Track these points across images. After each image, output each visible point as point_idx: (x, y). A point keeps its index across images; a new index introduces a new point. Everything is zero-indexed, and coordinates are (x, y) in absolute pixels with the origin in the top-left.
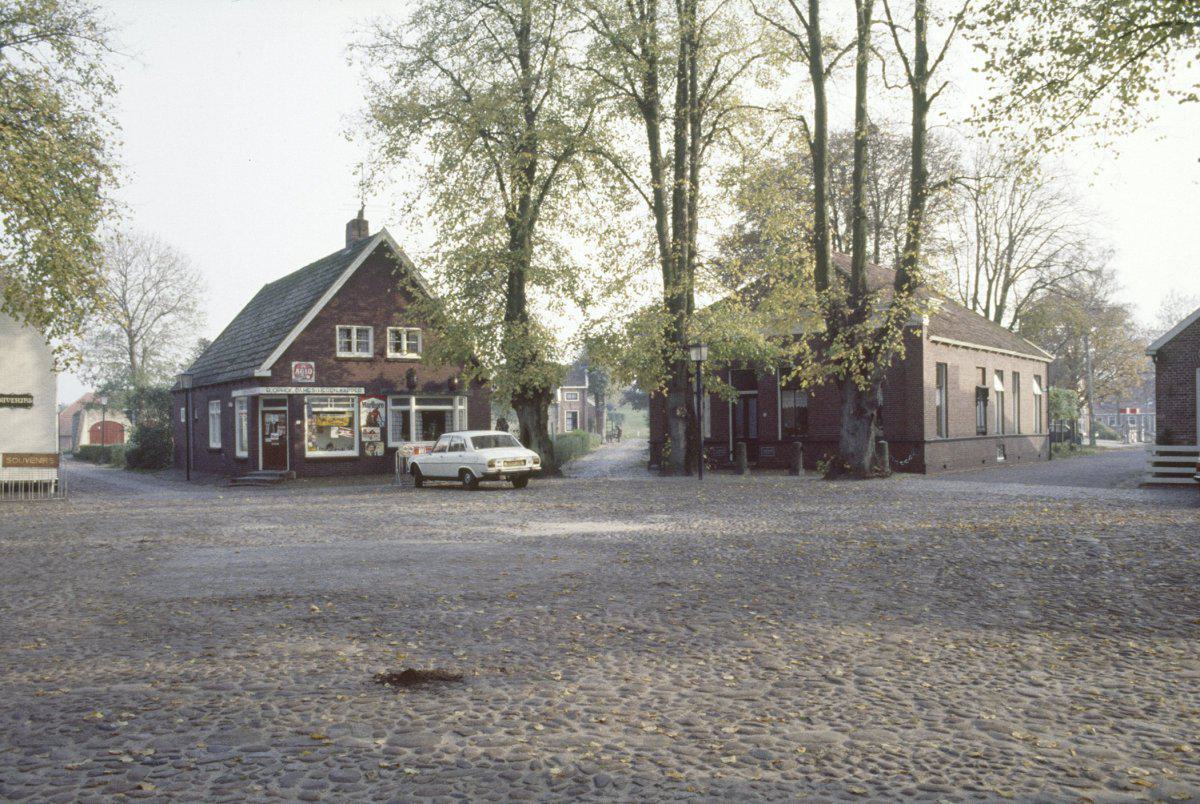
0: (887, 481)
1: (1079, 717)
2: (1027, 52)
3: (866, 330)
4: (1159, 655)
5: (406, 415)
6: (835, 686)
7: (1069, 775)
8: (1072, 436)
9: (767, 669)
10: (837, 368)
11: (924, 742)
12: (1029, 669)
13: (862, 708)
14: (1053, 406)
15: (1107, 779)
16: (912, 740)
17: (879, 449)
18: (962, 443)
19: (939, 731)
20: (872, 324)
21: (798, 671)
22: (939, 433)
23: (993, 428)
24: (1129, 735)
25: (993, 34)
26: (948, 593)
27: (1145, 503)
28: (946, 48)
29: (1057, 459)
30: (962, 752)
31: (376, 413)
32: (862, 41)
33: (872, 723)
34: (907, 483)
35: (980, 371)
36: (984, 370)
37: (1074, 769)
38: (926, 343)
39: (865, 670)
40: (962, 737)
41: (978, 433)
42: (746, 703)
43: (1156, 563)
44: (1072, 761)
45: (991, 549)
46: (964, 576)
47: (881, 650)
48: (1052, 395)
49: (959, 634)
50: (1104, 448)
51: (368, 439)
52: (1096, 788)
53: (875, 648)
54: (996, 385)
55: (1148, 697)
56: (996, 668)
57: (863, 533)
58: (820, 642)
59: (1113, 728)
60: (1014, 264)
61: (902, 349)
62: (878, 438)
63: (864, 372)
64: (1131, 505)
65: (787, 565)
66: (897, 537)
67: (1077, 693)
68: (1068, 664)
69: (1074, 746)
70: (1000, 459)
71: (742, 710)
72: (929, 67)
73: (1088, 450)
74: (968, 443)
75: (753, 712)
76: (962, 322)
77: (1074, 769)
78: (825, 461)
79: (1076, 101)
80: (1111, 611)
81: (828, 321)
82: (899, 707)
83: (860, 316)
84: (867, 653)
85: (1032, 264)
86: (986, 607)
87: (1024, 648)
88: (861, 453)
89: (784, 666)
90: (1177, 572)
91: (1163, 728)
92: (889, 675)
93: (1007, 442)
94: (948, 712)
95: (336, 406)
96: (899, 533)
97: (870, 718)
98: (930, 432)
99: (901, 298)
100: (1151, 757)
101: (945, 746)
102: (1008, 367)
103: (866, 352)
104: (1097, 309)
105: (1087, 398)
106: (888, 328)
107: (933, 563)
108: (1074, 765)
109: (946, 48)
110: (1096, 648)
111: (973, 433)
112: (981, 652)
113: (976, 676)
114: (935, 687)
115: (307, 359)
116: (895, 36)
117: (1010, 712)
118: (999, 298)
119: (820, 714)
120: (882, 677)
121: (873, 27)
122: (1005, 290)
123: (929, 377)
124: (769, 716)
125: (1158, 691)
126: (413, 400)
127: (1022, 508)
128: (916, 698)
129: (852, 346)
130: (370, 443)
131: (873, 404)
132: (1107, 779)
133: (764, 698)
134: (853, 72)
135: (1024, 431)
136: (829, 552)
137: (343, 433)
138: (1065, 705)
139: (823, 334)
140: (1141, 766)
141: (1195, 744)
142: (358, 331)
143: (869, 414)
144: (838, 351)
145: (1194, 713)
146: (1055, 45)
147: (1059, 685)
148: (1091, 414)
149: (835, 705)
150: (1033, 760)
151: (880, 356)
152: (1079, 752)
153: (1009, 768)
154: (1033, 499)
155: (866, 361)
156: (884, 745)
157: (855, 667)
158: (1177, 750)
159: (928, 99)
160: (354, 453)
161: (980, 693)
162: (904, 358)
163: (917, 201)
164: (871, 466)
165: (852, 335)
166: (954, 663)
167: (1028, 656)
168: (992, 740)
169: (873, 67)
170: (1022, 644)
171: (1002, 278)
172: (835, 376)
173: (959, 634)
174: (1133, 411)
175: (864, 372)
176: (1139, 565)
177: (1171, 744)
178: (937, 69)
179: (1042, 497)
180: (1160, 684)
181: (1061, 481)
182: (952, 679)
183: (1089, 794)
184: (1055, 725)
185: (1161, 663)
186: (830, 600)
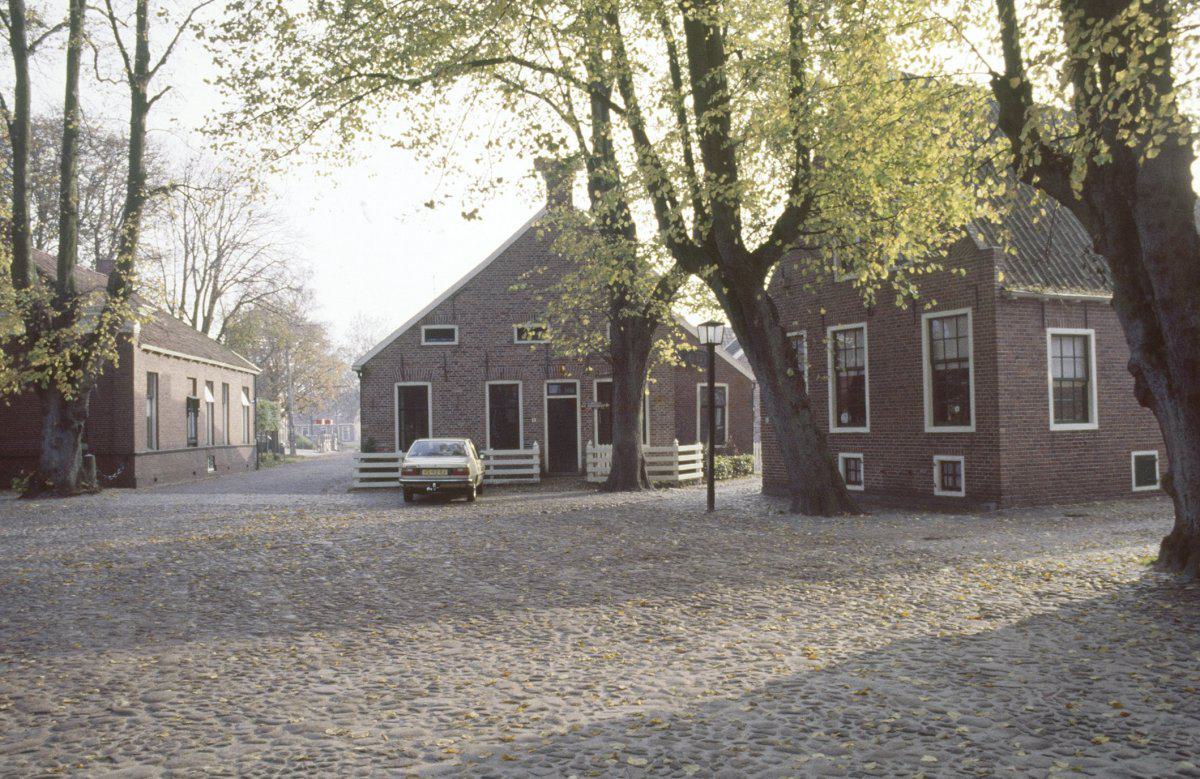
0: (95, 496)
1: (376, 705)
2: (259, 75)
3: (75, 335)
4: (422, 639)
6: (125, 719)
7: (390, 758)
8: (274, 445)
9: (36, 713)
10: (38, 376)
11: (246, 756)
12: (315, 669)
13: (166, 735)
14: (259, 416)
15: (422, 754)
16: (232, 757)
17: (86, 463)
18: (173, 455)
19: (254, 743)
20: (81, 329)
21: (76, 710)
22: (150, 445)
23: (204, 439)
24: (424, 711)
25: (234, 51)
26: (209, 607)
27: (359, 506)
28: (168, 52)
29: (263, 470)
30: (286, 759)
32: (75, 22)
33: (182, 748)
34: (116, 498)
35: (191, 382)
36: (194, 380)
37: (391, 751)
38: (137, 352)
39: (152, 696)
40: (280, 744)
41: (189, 445)
42: (24, 756)
43: (389, 560)
44: (387, 745)
45: (235, 559)
46: (218, 588)
47: (162, 673)
48: (258, 404)
49: (237, 645)
50: (303, 457)
52: (417, 764)
53: (154, 672)
54: (206, 396)
55: (427, 677)
56: (285, 674)
57: (91, 554)
58: (90, 675)
59: (410, 709)
60: (221, 279)
61: (115, 357)
62: (85, 452)
63: (72, 380)
64: (347, 509)
65: (13, 596)
66: (131, 555)
67: (366, 684)
68: (348, 659)
69: (383, 732)
70: (211, 470)
71: (23, 765)
72: (151, 67)
73: (290, 459)
74: (179, 456)
75: (39, 764)
76: (170, 331)
77: (391, 751)
78: (22, 478)
79: (300, 129)
80: (367, 607)
81: (27, 323)
82: (205, 727)
83: (67, 319)
84: (146, 678)
85: (240, 277)
86: (252, 616)
87: (304, 650)
88: (65, 467)
89: (55, 707)
90: (409, 565)
91: (450, 702)
92: (181, 696)
93: (217, 453)
94: (257, 722)
96: (131, 550)
97: (179, 744)
98: (140, 445)
99: (115, 303)
100: (450, 727)
101: (268, 756)
102: (218, 378)
103: (74, 358)
104: (296, 324)
105: (287, 409)
106: (99, 334)
107: (181, 580)
108: (391, 748)
109: (168, 52)
110: (367, 641)
111: (182, 443)
112: (264, 660)
113: (269, 683)
114: (234, 701)
116: (115, 28)
117: (315, 712)
118: (206, 310)
119: (120, 750)
120: (174, 700)
121: (88, 13)
122: (213, 302)
123: (140, 386)
124: (61, 765)
125: (432, 671)
127: (250, 516)
128: (218, 715)
129: (57, 352)
131: (80, 416)
132: (422, 754)
133: (45, 746)
134: (63, 57)
135: (234, 442)
136: (61, 578)
138: (360, 697)
139: (21, 337)
140: (445, 736)
141: (478, 709)
143: (76, 425)
144: (41, 356)
145: (467, 684)
146: (286, 73)
147: (347, 680)
148: (291, 425)
149: (134, 738)
150: (354, 751)
151: (90, 363)
152: (391, 736)
153: (336, 763)
154: (256, 508)
155: (74, 368)
156: (206, 768)
157: (140, 695)
158: (467, 718)
159: (148, 100)
161: (280, 699)
162: (117, 366)
163: (134, 205)
164: (78, 482)
165: (57, 340)
166: (243, 675)
167: (310, 657)
168: (308, 741)
169: (86, 57)
170: (301, 647)
171: (210, 289)
172: (37, 386)
173: (237, 645)
174: (328, 422)
175: (72, 380)
176: (374, 562)
177: (461, 713)
178: (158, 72)
179: (264, 506)
180: (431, 664)
181: (276, 489)
182: (247, 690)
183: (413, 770)
184: (359, 716)
185: (424, 647)
186: (82, 628)
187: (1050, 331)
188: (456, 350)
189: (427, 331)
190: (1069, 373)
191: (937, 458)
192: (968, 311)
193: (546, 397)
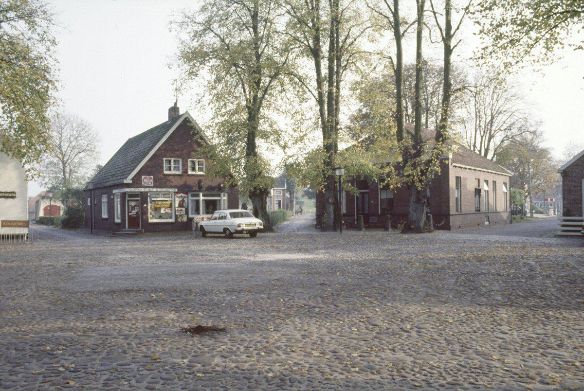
0: (431, 234)
1: (525, 349)
2: (500, 25)
3: (422, 160)
4: (564, 318)
5: (198, 202)
6: (407, 334)
7: (520, 377)
8: (522, 212)
9: (373, 325)
10: (407, 179)
11: (450, 361)
12: (501, 325)
13: (420, 344)
14: (512, 197)
15: (539, 379)
16: (444, 360)
17: (428, 218)
18: (468, 215)
19: (457, 355)
20: (424, 158)
21: (389, 326)
22: (457, 211)
23: (483, 208)
24: (550, 357)
25: (483, 17)
26: (462, 288)
27: (557, 245)
28: (460, 23)
29: (515, 223)
30: (468, 366)
31: (183, 201)
32: (420, 20)
33: (425, 351)
34: (441, 235)
35: (477, 181)
36: (479, 180)
37: (523, 374)
38: (451, 167)
39: (421, 326)
40: (468, 359)
41: (476, 211)
42: (363, 342)
43: (563, 274)
44: (522, 370)
45: (482, 267)
46: (469, 280)
47: (429, 316)
48: (512, 192)
49: (467, 308)
50: (537, 218)
51: (179, 214)
52: (533, 383)
53: (426, 315)
54: (485, 187)
55: (559, 339)
56: (485, 325)
57: (420, 259)
58: (399, 312)
59: (542, 354)
60: (493, 129)
61: (439, 170)
62: (427, 213)
63: (421, 181)
64: (550, 245)
65: (383, 275)
66: (437, 261)
67: (524, 337)
68: (520, 323)
69: (523, 363)
70: (487, 223)
71: (361, 345)
72: (452, 33)
73: (529, 219)
74: (471, 215)
75: (367, 346)
76: (468, 157)
77: (523, 374)
78: (402, 224)
79: (524, 49)
80: (541, 297)
81: (403, 156)
82: (438, 344)
83: (419, 154)
84: (422, 317)
85: (502, 128)
86: (480, 295)
87: (499, 315)
88: (419, 220)
89: (381, 324)
90: (573, 278)
91: (566, 354)
92: (433, 328)
93: (490, 215)
94: (462, 346)
95: (163, 197)
96: (437, 259)
97: (424, 349)
98: (453, 210)
99: (439, 145)
100: (560, 368)
101: (460, 363)
102: (491, 178)
103: (422, 171)
104: (534, 151)
105: (529, 194)
106: (432, 160)
107: (454, 274)
108: (523, 372)
109: (460, 23)
110: (533, 315)
111: (473, 211)
112: (477, 317)
113: (475, 329)
114: (455, 334)
115: (149, 175)
116: (436, 17)
117: (492, 346)
118: (486, 145)
119: (399, 347)
120: (429, 329)
121: (425, 13)
122: (489, 141)
123: (452, 183)
124: (374, 348)
125: (564, 336)
126: (201, 194)
127: (498, 247)
128: (446, 340)
129: (415, 168)
130: (180, 215)
131: (425, 197)
132: (539, 379)
133: (372, 339)
134: (415, 35)
135: (498, 210)
136: (404, 269)
137: (167, 211)
138: (518, 343)
139: (401, 163)
140: (555, 372)
141: (581, 362)
142: (174, 161)
143: (423, 201)
144: (408, 171)
145: (581, 347)
146: (514, 22)
147: (515, 333)
148: (531, 201)
149: (406, 343)
150: (503, 369)
151: (428, 173)
152: (525, 366)
153: (491, 373)
154: (503, 243)
155: (422, 175)
156: (430, 362)
157: (416, 325)
158: (573, 365)
159: (451, 48)
160: (172, 220)
161: (477, 337)
162: (440, 174)
163: (446, 98)
164: (424, 227)
165: (415, 163)
166: (464, 323)
167: (500, 319)
168: (483, 360)
169: (425, 33)
170: (498, 313)
171: (488, 135)
172: (407, 183)
173: (467, 308)
174: (552, 200)
175: (421, 181)
176: (554, 275)
177: (570, 362)
178: (456, 34)
179: (507, 242)
180: (565, 332)
181: (516, 234)
182: (464, 330)
183: (530, 386)
184: (513, 352)
185: (565, 323)
186: (404, 292)
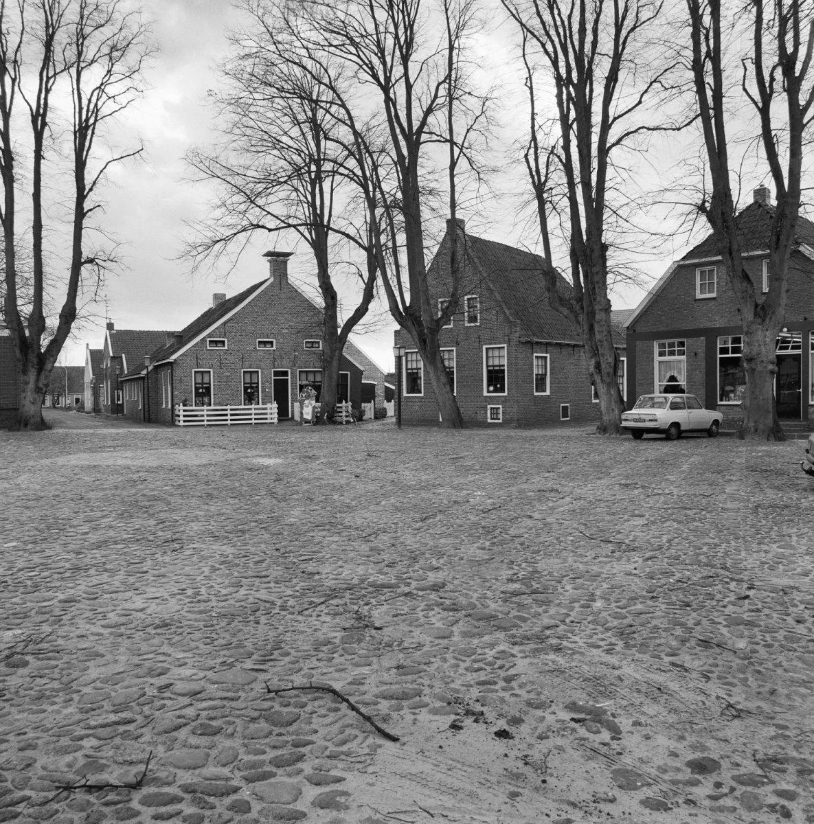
187: (535, 354)
188: (226, 352)
189: (210, 341)
190: (540, 372)
191: (489, 407)
192: (505, 345)
193: (273, 378)
